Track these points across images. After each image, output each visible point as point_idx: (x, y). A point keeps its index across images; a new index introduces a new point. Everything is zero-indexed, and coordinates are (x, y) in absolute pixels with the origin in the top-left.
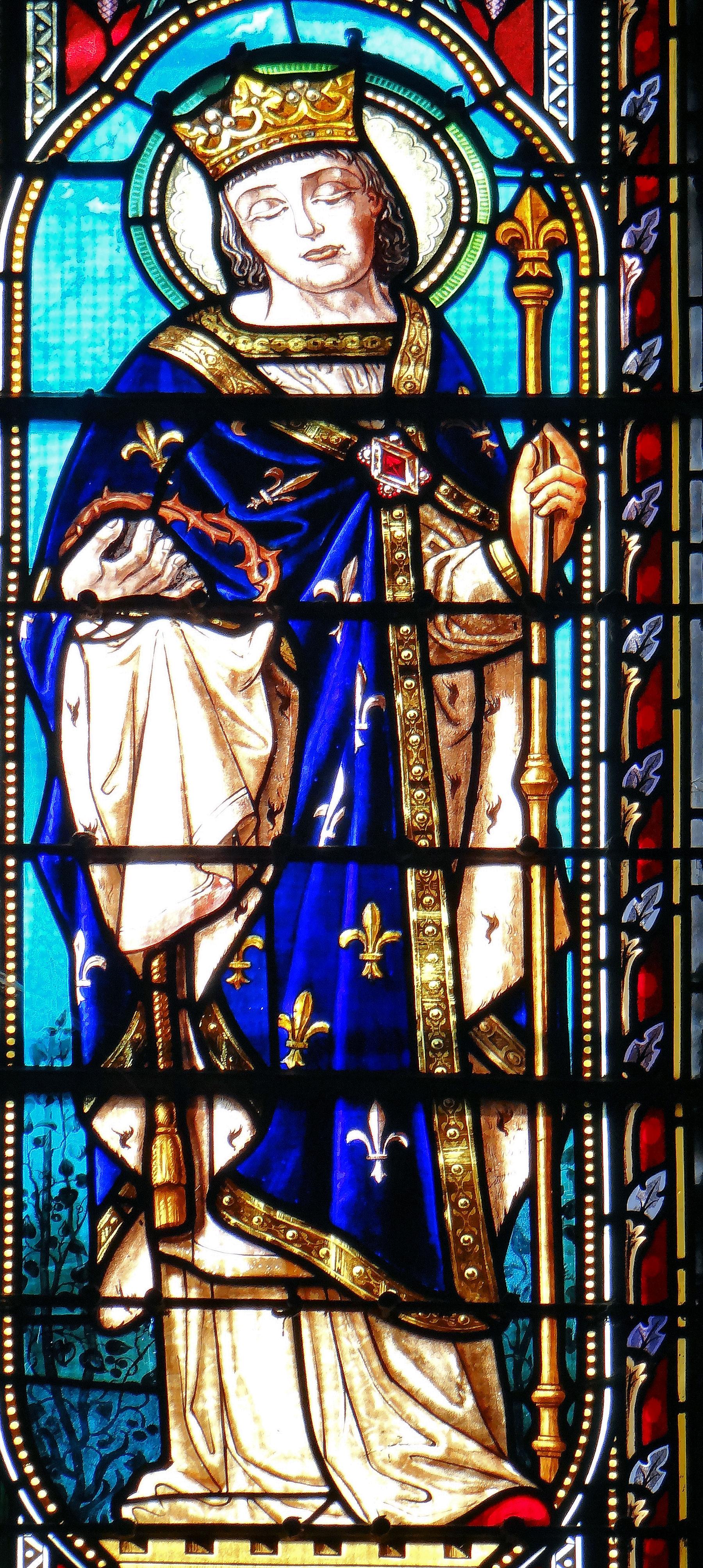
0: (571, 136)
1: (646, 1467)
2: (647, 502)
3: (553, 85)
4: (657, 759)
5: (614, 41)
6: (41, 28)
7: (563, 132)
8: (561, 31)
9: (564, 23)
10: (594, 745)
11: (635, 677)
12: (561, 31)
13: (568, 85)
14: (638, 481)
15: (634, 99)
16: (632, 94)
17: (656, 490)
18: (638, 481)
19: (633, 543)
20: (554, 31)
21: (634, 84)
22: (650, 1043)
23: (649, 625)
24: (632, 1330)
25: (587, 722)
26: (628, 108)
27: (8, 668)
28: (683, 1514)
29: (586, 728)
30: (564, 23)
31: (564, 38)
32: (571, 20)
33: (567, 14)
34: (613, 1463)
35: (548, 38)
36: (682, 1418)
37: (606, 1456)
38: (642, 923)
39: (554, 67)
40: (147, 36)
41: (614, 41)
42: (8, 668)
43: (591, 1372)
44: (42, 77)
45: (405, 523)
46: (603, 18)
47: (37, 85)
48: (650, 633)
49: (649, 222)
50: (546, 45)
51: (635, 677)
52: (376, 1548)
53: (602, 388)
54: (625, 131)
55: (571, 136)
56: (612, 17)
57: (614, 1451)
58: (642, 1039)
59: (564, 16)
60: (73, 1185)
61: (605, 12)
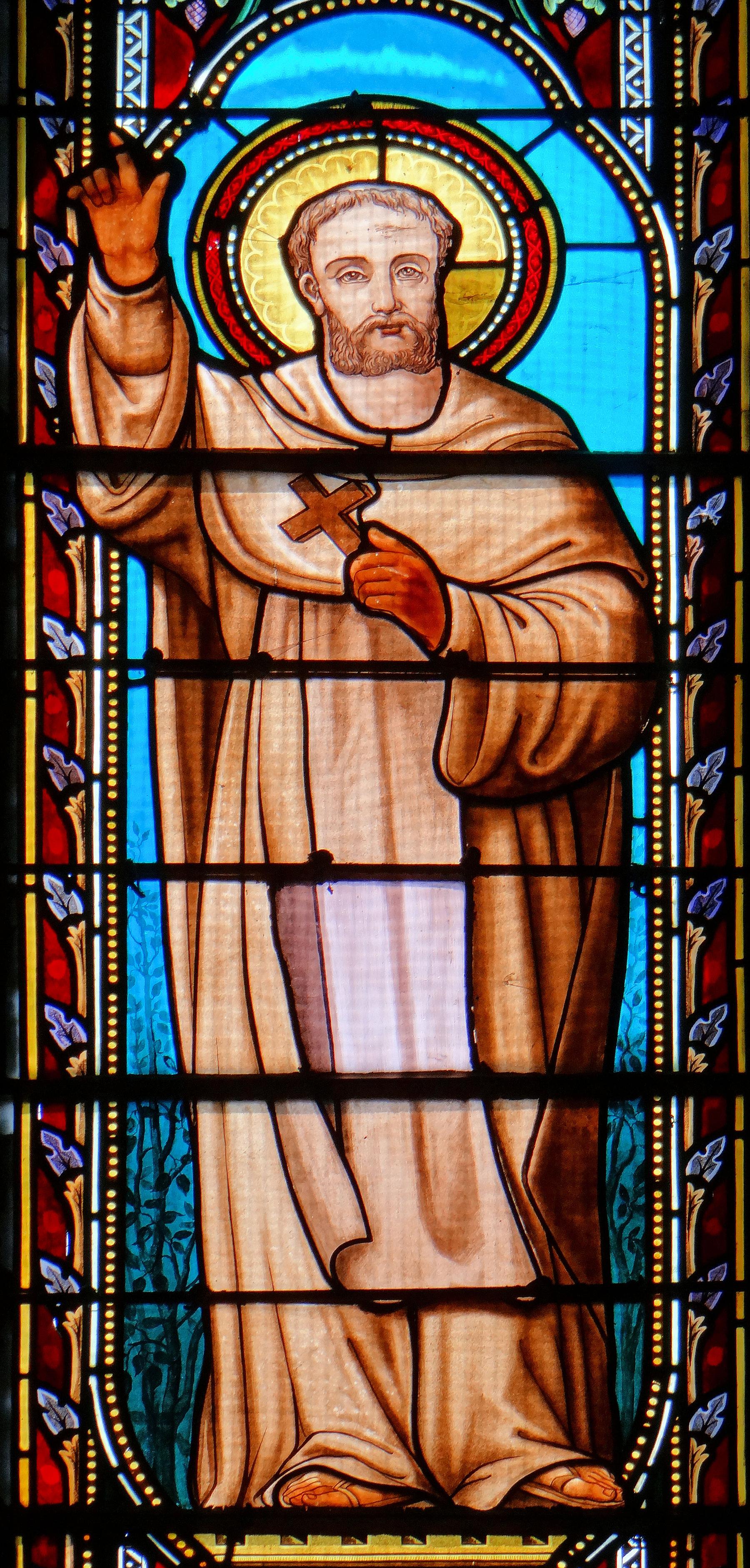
0: (648, 162)
1: (707, 1413)
2: (713, 1023)
3: (629, 65)
4: (725, 237)
5: (687, 67)
6: (129, 41)
7: (639, 160)
8: (637, 48)
9: (640, 40)
10: (665, 769)
11: (700, 808)
12: (637, 48)
13: (644, 99)
14: (705, 1001)
15: (705, 250)
16: (705, 244)
17: (721, 628)
18: (705, 1001)
19: (704, 416)
20: (630, 47)
21: (707, 235)
22: (713, 1023)
23: (715, 1013)
24: (693, 1414)
25: (657, 520)
26: (695, 1033)
27: (89, 89)
28: (742, 1067)
29: (656, 514)
30: (640, 40)
31: (640, 55)
32: (647, 38)
33: (643, 31)
34: (675, 1440)
35: (624, 54)
36: (740, 972)
37: (669, 1434)
38: (704, 1176)
39: (630, 82)
40: (227, 177)
41: (687, 67)
42: (90, 42)
43: (657, 1361)
44: (133, 51)
45: (470, 1436)
46: (676, 46)
47: (127, 27)
48: (713, 1155)
49: (716, 632)
50: (622, 60)
51: (700, 808)
52: (459, 1538)
53: (673, 445)
54: (696, 22)
55: (648, 162)
56: (685, 45)
57: (676, 1429)
58: (711, 243)
59: (639, 34)
60: (175, 1240)
61: (678, 39)
